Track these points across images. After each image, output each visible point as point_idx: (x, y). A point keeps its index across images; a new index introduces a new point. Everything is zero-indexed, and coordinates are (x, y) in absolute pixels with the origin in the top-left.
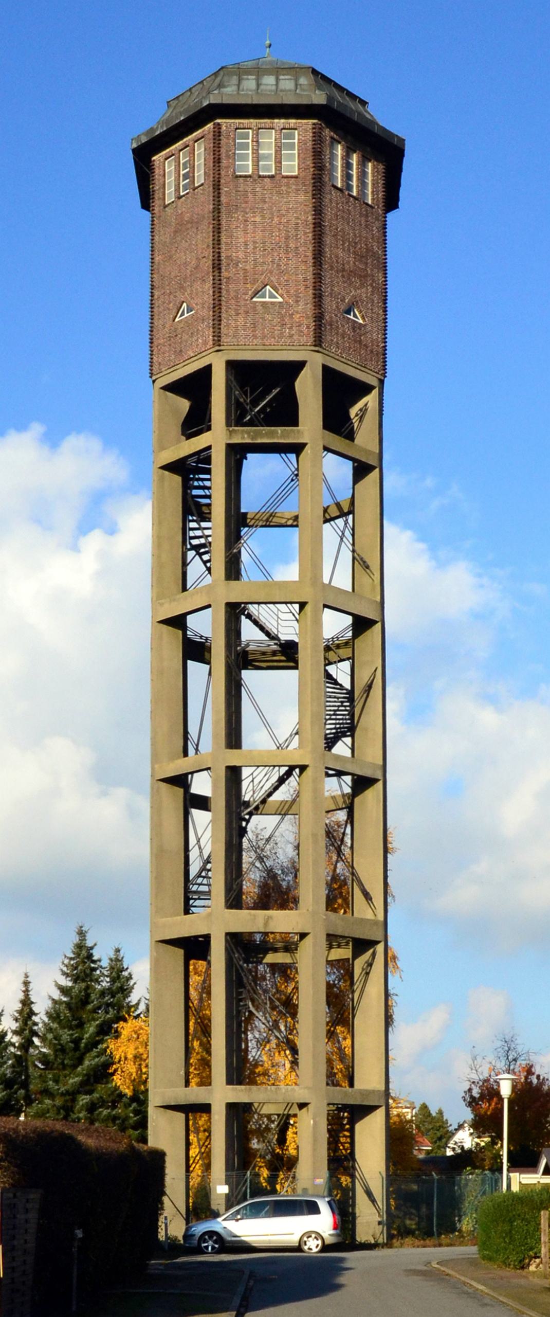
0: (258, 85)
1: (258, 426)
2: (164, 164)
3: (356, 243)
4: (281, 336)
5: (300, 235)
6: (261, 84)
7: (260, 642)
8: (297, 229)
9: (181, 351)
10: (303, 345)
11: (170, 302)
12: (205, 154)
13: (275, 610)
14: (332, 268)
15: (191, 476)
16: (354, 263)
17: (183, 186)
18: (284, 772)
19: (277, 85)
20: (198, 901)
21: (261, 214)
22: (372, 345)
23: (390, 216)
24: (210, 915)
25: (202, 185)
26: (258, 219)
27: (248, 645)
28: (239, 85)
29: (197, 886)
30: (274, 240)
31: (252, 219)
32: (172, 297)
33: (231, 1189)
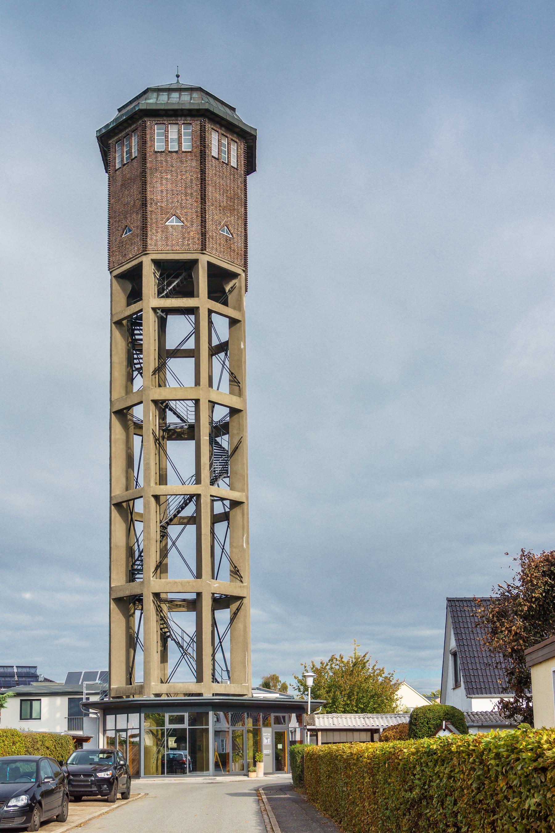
0: (169, 98)
3: (227, 191)
4: (183, 245)
5: (194, 185)
7: (175, 424)
8: (191, 182)
9: (125, 255)
10: (196, 250)
11: (119, 226)
13: (186, 405)
14: (213, 205)
16: (227, 202)
19: (180, 98)
24: (142, 582)
25: (136, 157)
26: (169, 177)
27: (169, 426)
28: (157, 98)
32: (120, 223)
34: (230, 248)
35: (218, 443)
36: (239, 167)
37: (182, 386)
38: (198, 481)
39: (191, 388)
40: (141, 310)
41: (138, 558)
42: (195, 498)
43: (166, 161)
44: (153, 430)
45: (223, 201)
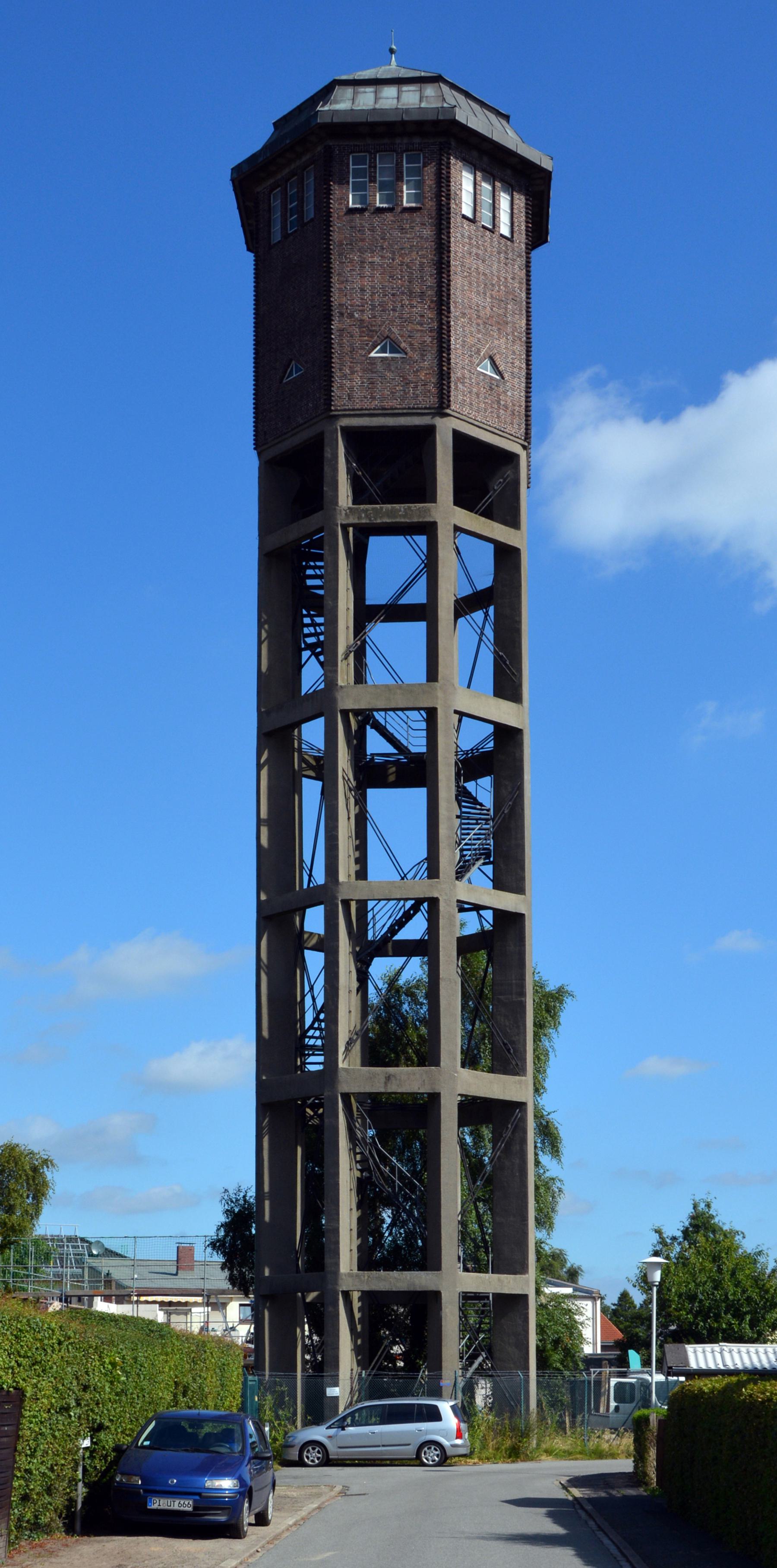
0: (376, 99)
1: (378, 503)
2: (270, 197)
3: (493, 285)
6: (380, 98)
13: (405, 718)
16: (492, 309)
17: (290, 222)
22: (514, 405)
23: (535, 254)
25: (312, 220)
26: (377, 259)
29: (314, 1040)
30: (396, 284)
31: (370, 260)
34: (498, 402)
35: (470, 793)
36: (515, 235)
37: (400, 682)
38: (433, 872)
39: (420, 685)
41: (313, 1023)
42: (425, 905)
43: (372, 230)
44: (343, 770)
45: (485, 307)
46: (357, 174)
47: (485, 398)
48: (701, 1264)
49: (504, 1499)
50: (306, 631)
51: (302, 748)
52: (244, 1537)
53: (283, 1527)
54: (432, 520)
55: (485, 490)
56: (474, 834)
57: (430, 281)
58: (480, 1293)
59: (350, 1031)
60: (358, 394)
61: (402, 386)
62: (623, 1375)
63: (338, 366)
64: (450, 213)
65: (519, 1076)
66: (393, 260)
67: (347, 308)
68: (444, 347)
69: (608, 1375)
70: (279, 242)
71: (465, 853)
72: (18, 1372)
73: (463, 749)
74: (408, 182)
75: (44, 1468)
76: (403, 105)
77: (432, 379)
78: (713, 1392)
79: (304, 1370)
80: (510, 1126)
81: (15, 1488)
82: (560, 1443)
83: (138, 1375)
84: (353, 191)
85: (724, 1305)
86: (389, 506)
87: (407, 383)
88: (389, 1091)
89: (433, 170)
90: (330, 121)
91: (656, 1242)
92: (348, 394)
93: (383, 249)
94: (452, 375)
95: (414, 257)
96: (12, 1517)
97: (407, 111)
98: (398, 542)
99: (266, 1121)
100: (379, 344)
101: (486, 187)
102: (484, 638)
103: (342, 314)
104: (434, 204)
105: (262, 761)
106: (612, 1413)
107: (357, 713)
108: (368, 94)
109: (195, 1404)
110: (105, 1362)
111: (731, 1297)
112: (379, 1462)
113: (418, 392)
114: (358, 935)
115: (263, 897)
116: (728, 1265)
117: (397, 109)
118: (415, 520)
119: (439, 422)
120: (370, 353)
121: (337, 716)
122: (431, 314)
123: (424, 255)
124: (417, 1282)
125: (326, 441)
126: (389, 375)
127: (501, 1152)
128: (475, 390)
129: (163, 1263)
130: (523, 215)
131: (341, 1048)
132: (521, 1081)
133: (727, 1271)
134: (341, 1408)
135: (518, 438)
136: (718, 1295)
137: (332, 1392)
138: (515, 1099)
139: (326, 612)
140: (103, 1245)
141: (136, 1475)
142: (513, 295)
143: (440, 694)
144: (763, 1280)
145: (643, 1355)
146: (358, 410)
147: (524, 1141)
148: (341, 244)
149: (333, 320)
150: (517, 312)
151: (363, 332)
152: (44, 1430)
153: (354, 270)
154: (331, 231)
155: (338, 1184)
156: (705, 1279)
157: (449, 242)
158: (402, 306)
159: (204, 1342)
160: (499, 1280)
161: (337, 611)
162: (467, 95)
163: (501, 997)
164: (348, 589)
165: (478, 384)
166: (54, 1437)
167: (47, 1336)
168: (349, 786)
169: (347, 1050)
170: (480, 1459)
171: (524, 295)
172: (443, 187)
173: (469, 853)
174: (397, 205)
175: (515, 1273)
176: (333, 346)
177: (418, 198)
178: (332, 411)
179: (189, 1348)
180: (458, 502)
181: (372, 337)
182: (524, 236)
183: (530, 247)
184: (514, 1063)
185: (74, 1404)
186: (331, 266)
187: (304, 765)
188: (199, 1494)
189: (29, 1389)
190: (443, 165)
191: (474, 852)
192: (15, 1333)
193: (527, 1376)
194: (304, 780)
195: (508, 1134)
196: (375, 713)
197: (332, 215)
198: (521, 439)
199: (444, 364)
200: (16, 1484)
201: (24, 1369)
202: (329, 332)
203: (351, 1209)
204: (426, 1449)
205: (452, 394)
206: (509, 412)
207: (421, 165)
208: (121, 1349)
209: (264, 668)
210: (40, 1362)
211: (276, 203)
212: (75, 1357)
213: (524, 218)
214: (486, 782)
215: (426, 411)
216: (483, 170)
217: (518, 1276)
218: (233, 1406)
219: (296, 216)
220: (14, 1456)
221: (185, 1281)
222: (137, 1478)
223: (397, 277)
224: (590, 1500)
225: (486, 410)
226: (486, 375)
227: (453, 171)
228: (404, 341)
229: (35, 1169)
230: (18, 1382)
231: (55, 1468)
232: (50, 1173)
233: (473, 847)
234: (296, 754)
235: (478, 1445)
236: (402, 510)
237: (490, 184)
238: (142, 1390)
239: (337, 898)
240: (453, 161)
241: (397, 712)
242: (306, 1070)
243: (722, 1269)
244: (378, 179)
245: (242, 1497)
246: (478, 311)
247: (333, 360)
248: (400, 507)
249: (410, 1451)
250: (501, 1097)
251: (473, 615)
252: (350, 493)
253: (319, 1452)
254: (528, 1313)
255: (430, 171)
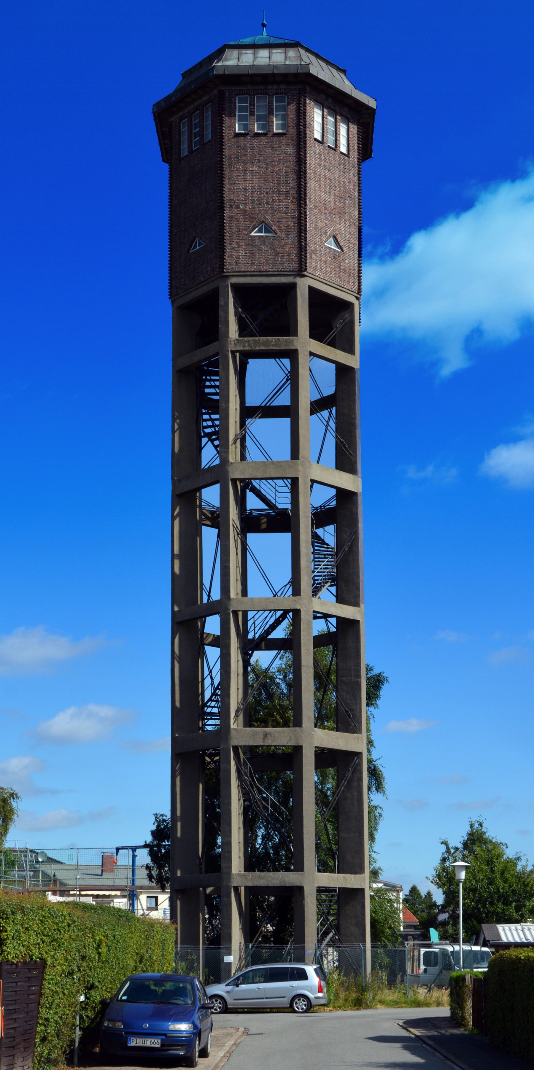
0: (255, 59)
1: (256, 336)
2: (180, 124)
3: (335, 187)
12: (212, 116)
14: (316, 207)
15: (204, 377)
16: (335, 204)
17: (195, 142)
18: (280, 615)
20: (210, 721)
21: (258, 164)
22: (350, 269)
23: (364, 165)
25: (210, 141)
29: (211, 708)
31: (251, 169)
33: (221, 960)
34: (340, 268)
35: (319, 537)
36: (350, 153)
37: (270, 460)
38: (296, 592)
39: (287, 462)
40: (217, 354)
41: (211, 697)
42: (291, 614)
43: (252, 148)
44: (233, 520)
46: (241, 109)
47: (331, 264)
48: (479, 866)
49: (367, 1037)
50: (205, 424)
51: (202, 505)
52: (196, 1066)
53: (219, 1059)
54: (294, 348)
55: (330, 328)
56: (324, 565)
57: (293, 184)
58: (329, 887)
59: (238, 702)
60: (242, 261)
61: (273, 256)
62: (429, 946)
63: (228, 242)
64: (306, 137)
65: (357, 733)
66: (267, 169)
67: (235, 202)
68: (302, 229)
69: (412, 946)
70: (186, 156)
71: (316, 578)
72: (43, 947)
73: (315, 506)
74: (277, 115)
75: (57, 1017)
76: (273, 62)
77: (294, 251)
78: (528, 959)
79: (204, 944)
80: (350, 769)
81: (38, 1032)
82: (389, 995)
83: (116, 948)
84: (238, 122)
85: (496, 895)
86: (264, 338)
87: (276, 254)
88: (267, 744)
89: (294, 107)
90: (223, 73)
91: (444, 851)
92: (236, 261)
93: (260, 161)
94: (308, 248)
95: (282, 168)
96: (36, 1053)
97: (276, 67)
98: (270, 363)
99: (178, 765)
100: (257, 227)
101: (331, 119)
102: (329, 428)
103: (231, 206)
104: (295, 131)
105: (175, 514)
106: (422, 974)
107: (242, 480)
108: (248, 55)
109: (147, 969)
110: (96, 939)
111: (501, 891)
112: (262, 1010)
113: (284, 260)
114: (242, 634)
115: (176, 609)
116: (498, 868)
117: (269, 65)
118: (283, 348)
119: (299, 281)
120: (251, 233)
121: (229, 483)
122: (293, 207)
123: (288, 166)
124: (287, 880)
125: (221, 293)
126: (264, 248)
127: (344, 788)
128: (323, 259)
129: (92, 867)
130: (356, 138)
131: (232, 715)
132: (358, 737)
133: (498, 872)
134: (233, 971)
135: (353, 292)
136: (492, 889)
137: (228, 959)
138: (354, 750)
139: (220, 411)
140: (46, 854)
141: (119, 1021)
142: (349, 193)
143: (300, 468)
144: (524, 878)
145: (440, 932)
146: (242, 272)
147: (360, 780)
148: (230, 158)
149: (225, 210)
150: (352, 205)
151: (246, 218)
152: (58, 989)
153: (239, 176)
154: (224, 149)
155: (230, 810)
156: (483, 877)
157: (306, 157)
158: (273, 201)
159: (152, 923)
160: (344, 878)
161: (229, 410)
162: (317, 56)
163: (344, 679)
164: (236, 395)
165: (325, 254)
166: (64, 994)
167: (61, 920)
168: (237, 531)
169: (236, 716)
170: (334, 1007)
171: (356, 194)
172: (301, 119)
173: (321, 578)
174: (269, 131)
175: (355, 873)
176: (225, 228)
177: (283, 126)
178: (225, 272)
179: (144, 928)
180: (312, 336)
181: (252, 222)
182: (356, 153)
183: (360, 161)
184: (353, 724)
185: (77, 970)
186: (224, 172)
187: (203, 517)
188: (165, 1035)
189: (49, 959)
190: (301, 104)
191: (324, 577)
192: (41, 919)
193: (365, 946)
194: (203, 527)
195: (349, 775)
196: (253, 481)
197: (224, 138)
198: (355, 292)
199: (302, 240)
200: (39, 1029)
201: (46, 944)
202: (222, 218)
203: (239, 828)
204: (297, 1000)
205: (308, 261)
206: (347, 274)
207: (286, 104)
208: (106, 929)
209: (176, 450)
210: (57, 940)
211: (184, 129)
212: (78, 936)
213: (356, 141)
214: (331, 529)
215: (290, 273)
216: (328, 108)
217: (357, 875)
218: (169, 970)
219: (198, 138)
220: (38, 1008)
221: (107, 880)
222: (120, 1024)
223: (270, 181)
224: (429, 1037)
225: (331, 273)
226: (331, 248)
227: (308, 108)
228: (275, 225)
229: (4, 800)
230: (42, 955)
231: (63, 1017)
232: (16, 802)
233: (323, 574)
234: (198, 509)
235: (332, 997)
236: (274, 341)
237: (333, 118)
238: (118, 959)
239: (229, 610)
240: (308, 101)
241: (268, 480)
242: (205, 729)
243: (494, 870)
244: (256, 113)
245: (195, 1037)
246: (325, 205)
247: (225, 238)
248: (272, 339)
249: (285, 1002)
250: (344, 749)
251: (322, 413)
252: (237, 330)
253: (220, 1003)
254: (364, 902)
255: (292, 108)
